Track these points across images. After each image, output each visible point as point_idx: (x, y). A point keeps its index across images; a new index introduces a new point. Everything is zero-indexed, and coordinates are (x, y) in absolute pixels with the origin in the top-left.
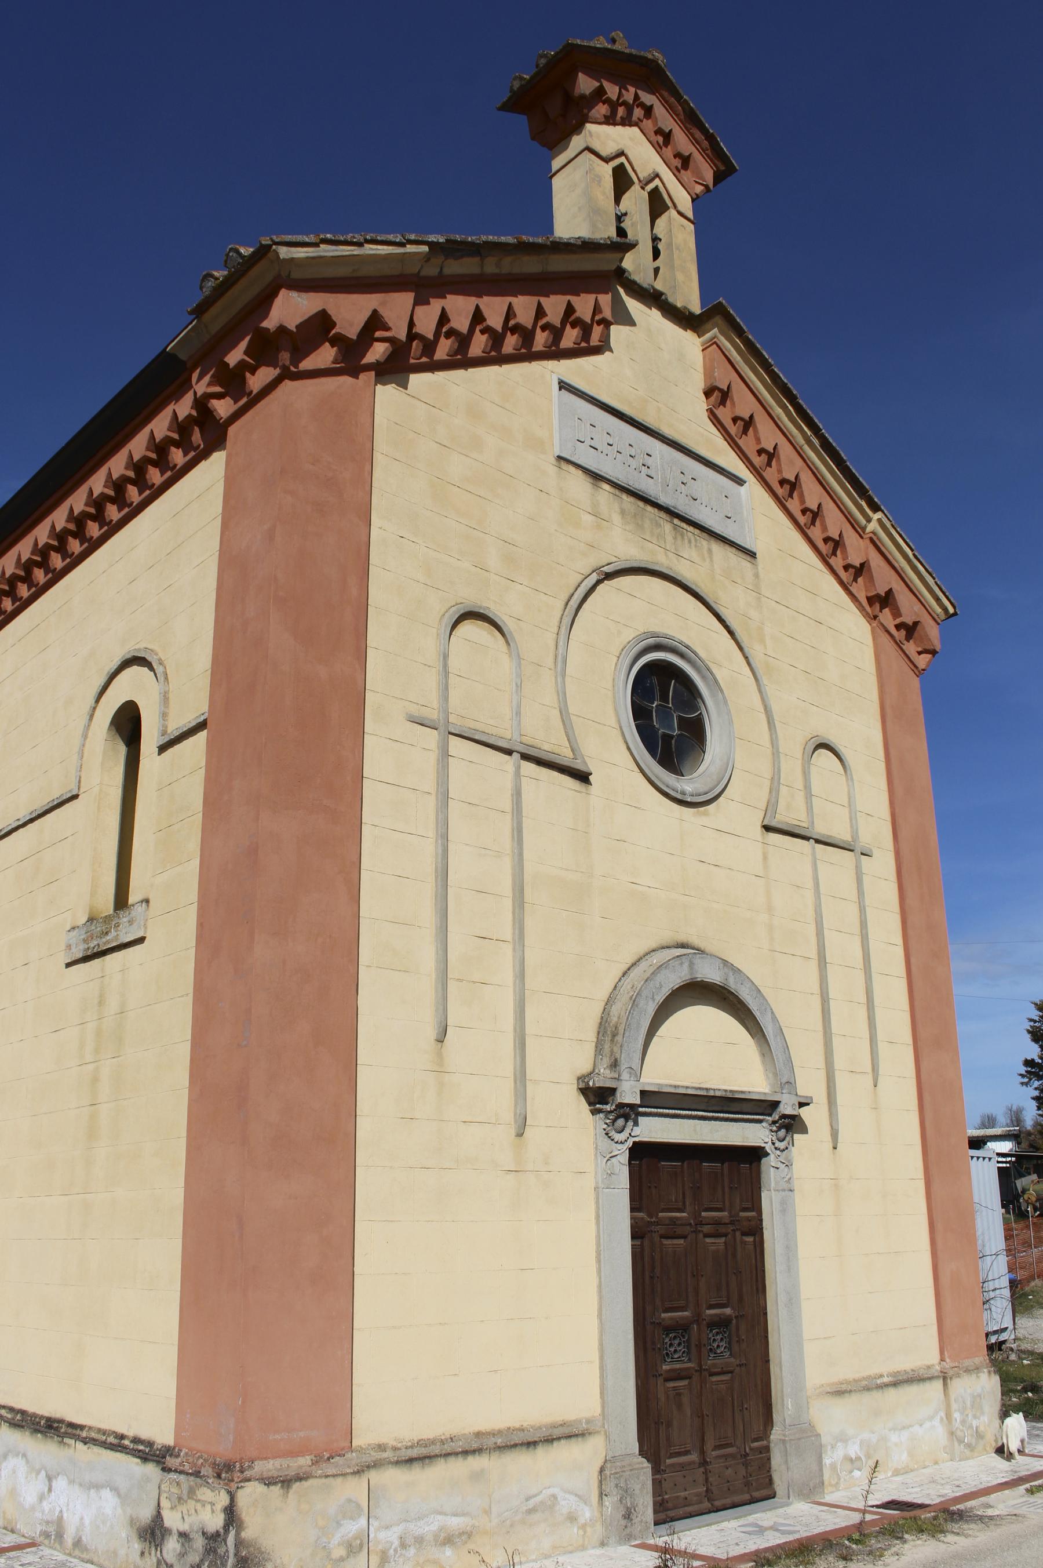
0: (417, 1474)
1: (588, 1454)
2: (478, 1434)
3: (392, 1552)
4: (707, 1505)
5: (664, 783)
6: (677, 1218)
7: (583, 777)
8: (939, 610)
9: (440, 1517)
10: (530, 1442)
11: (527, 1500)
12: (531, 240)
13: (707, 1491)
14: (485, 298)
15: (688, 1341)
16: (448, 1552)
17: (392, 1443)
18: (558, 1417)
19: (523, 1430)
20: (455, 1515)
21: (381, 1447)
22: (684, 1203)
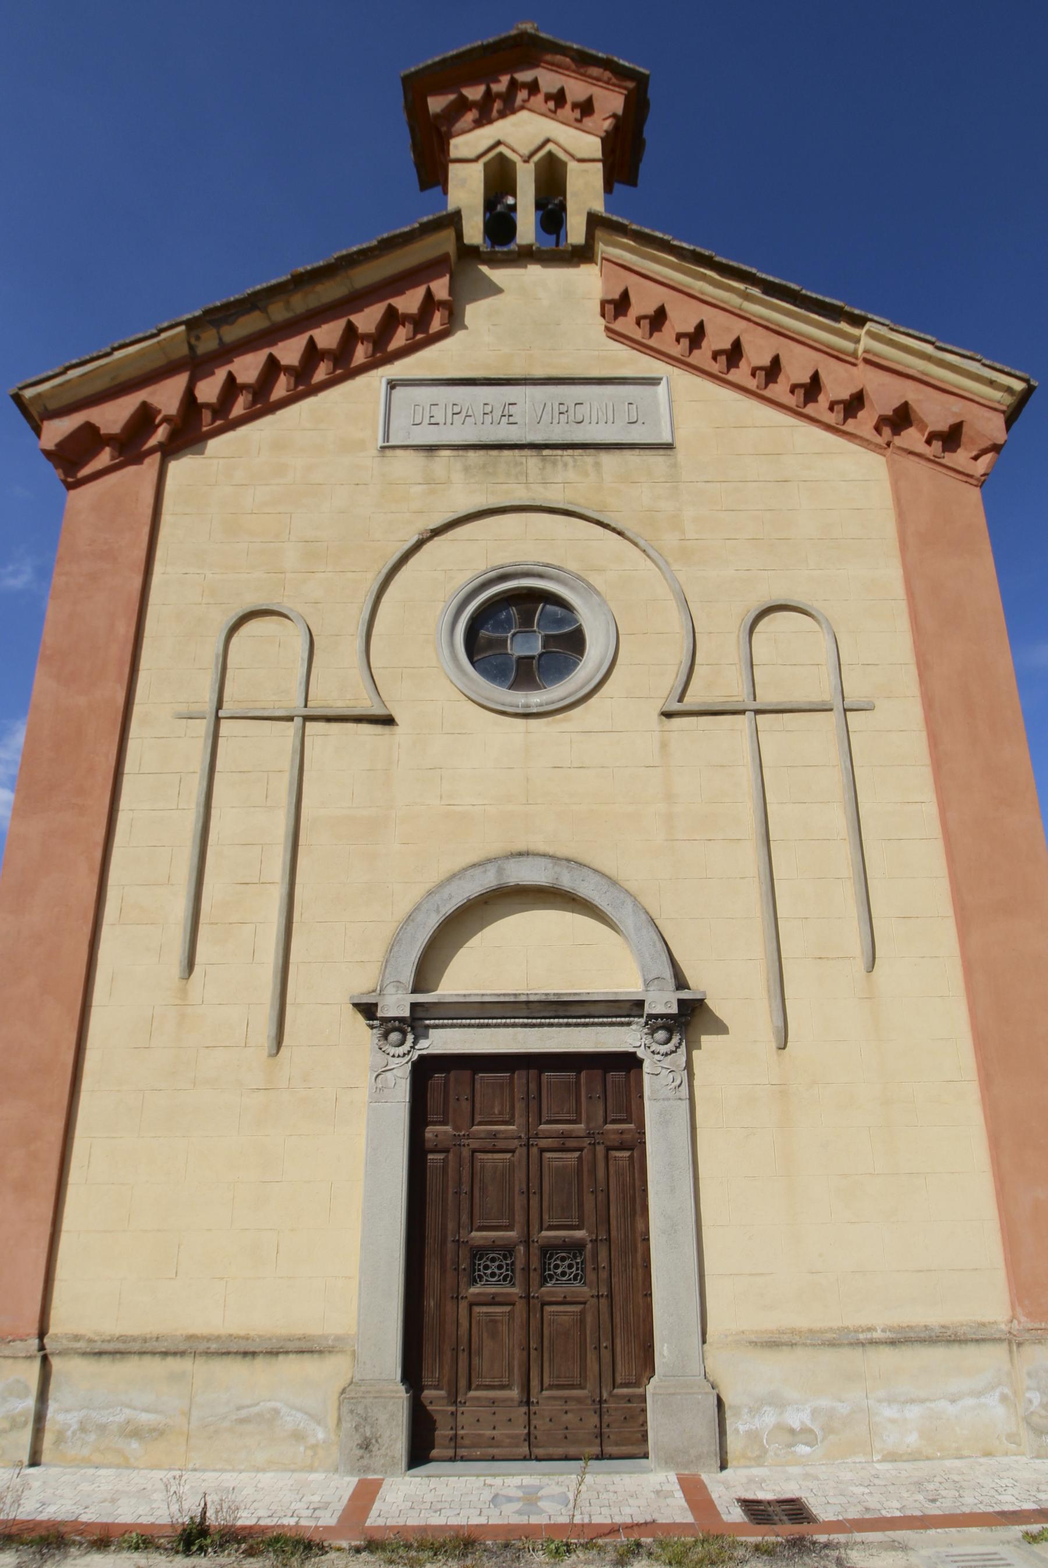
0: (105, 1365)
1: (329, 1375)
2: (190, 1338)
3: (69, 1433)
4: (525, 1450)
5: (497, 703)
6: (499, 1132)
7: (388, 721)
8: (998, 395)
9: (127, 1411)
10: (247, 1352)
11: (238, 1409)
12: (309, 268)
13: (529, 1434)
14: (281, 344)
15: (513, 1263)
16: (135, 1445)
17: (90, 1335)
18: (298, 1331)
19: (248, 1339)
20: (146, 1410)
21: (77, 1338)
22: (513, 1116)
